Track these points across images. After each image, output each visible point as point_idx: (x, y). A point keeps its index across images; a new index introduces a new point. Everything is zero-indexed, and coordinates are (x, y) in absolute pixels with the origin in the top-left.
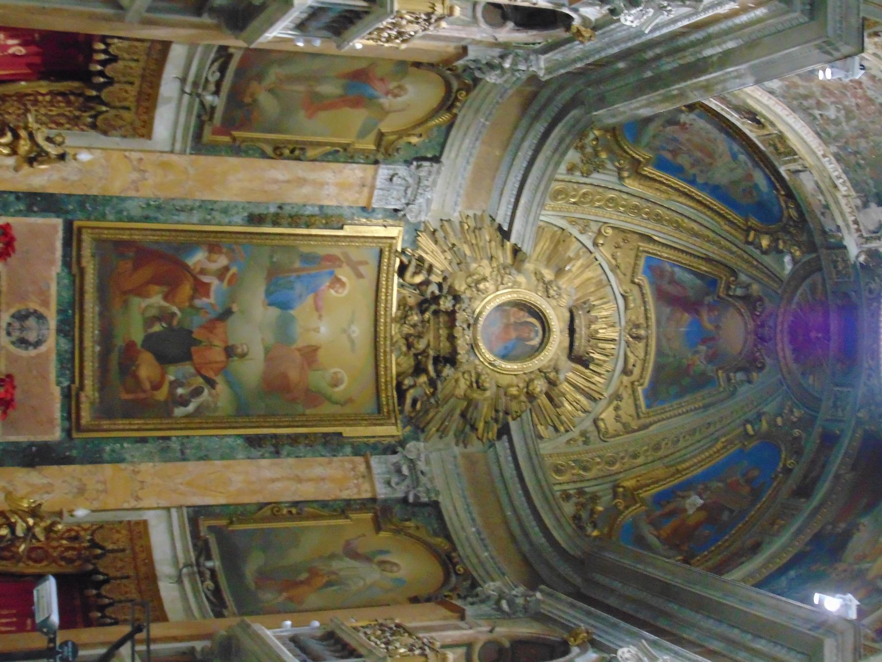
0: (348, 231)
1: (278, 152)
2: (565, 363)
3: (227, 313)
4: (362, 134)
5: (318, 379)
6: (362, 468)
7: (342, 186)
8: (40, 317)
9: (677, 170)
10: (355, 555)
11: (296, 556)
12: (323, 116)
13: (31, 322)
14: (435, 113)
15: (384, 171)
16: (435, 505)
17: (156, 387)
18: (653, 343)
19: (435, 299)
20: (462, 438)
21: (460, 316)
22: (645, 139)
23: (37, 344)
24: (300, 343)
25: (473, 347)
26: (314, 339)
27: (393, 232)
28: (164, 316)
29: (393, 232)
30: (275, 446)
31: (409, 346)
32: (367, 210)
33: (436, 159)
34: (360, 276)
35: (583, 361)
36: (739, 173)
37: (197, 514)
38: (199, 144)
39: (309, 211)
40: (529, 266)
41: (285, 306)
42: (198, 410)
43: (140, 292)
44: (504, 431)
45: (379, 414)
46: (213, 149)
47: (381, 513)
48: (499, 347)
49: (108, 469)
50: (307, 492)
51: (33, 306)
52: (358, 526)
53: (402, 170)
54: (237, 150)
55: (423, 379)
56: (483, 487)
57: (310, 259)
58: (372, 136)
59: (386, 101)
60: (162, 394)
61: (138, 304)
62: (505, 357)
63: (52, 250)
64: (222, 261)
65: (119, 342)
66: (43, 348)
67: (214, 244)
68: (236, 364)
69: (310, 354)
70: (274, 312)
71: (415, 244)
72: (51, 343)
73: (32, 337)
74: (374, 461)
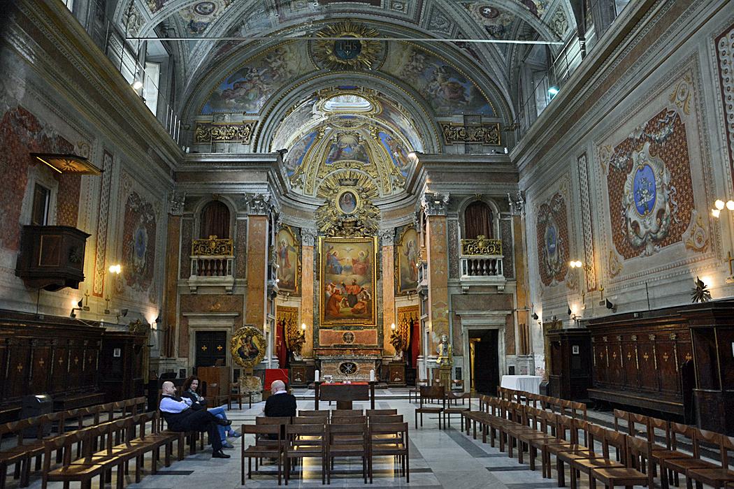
0: (320, 252)
1: (300, 273)
2: (357, 187)
4: (294, 251)
5: (362, 259)
6: (386, 248)
8: (345, 334)
9: (301, 158)
10: (408, 253)
11: (408, 268)
13: (346, 337)
14: (288, 231)
15: (304, 243)
16: (396, 228)
17: (364, 304)
19: (339, 227)
20: (378, 218)
21: (344, 220)
22: (292, 168)
25: (351, 215)
26: (350, 260)
27: (320, 239)
28: (344, 302)
29: (320, 239)
30: (379, 272)
31: (352, 233)
32: (315, 246)
33: (300, 229)
34: (332, 248)
35: (356, 181)
36: (303, 143)
37: (396, 294)
38: (300, 295)
39: (315, 264)
41: (341, 269)
43: (338, 308)
44: (376, 206)
45: (371, 242)
46: (300, 291)
50: (391, 264)
52: (402, 251)
53: (303, 238)
55: (361, 230)
56: (391, 214)
58: (295, 248)
59: (286, 246)
60: (365, 302)
62: (356, 204)
63: (327, 332)
64: (329, 286)
66: (353, 334)
68: (357, 282)
69: (354, 262)
71: (324, 232)
72: (351, 332)
73: (351, 336)
74: (384, 245)
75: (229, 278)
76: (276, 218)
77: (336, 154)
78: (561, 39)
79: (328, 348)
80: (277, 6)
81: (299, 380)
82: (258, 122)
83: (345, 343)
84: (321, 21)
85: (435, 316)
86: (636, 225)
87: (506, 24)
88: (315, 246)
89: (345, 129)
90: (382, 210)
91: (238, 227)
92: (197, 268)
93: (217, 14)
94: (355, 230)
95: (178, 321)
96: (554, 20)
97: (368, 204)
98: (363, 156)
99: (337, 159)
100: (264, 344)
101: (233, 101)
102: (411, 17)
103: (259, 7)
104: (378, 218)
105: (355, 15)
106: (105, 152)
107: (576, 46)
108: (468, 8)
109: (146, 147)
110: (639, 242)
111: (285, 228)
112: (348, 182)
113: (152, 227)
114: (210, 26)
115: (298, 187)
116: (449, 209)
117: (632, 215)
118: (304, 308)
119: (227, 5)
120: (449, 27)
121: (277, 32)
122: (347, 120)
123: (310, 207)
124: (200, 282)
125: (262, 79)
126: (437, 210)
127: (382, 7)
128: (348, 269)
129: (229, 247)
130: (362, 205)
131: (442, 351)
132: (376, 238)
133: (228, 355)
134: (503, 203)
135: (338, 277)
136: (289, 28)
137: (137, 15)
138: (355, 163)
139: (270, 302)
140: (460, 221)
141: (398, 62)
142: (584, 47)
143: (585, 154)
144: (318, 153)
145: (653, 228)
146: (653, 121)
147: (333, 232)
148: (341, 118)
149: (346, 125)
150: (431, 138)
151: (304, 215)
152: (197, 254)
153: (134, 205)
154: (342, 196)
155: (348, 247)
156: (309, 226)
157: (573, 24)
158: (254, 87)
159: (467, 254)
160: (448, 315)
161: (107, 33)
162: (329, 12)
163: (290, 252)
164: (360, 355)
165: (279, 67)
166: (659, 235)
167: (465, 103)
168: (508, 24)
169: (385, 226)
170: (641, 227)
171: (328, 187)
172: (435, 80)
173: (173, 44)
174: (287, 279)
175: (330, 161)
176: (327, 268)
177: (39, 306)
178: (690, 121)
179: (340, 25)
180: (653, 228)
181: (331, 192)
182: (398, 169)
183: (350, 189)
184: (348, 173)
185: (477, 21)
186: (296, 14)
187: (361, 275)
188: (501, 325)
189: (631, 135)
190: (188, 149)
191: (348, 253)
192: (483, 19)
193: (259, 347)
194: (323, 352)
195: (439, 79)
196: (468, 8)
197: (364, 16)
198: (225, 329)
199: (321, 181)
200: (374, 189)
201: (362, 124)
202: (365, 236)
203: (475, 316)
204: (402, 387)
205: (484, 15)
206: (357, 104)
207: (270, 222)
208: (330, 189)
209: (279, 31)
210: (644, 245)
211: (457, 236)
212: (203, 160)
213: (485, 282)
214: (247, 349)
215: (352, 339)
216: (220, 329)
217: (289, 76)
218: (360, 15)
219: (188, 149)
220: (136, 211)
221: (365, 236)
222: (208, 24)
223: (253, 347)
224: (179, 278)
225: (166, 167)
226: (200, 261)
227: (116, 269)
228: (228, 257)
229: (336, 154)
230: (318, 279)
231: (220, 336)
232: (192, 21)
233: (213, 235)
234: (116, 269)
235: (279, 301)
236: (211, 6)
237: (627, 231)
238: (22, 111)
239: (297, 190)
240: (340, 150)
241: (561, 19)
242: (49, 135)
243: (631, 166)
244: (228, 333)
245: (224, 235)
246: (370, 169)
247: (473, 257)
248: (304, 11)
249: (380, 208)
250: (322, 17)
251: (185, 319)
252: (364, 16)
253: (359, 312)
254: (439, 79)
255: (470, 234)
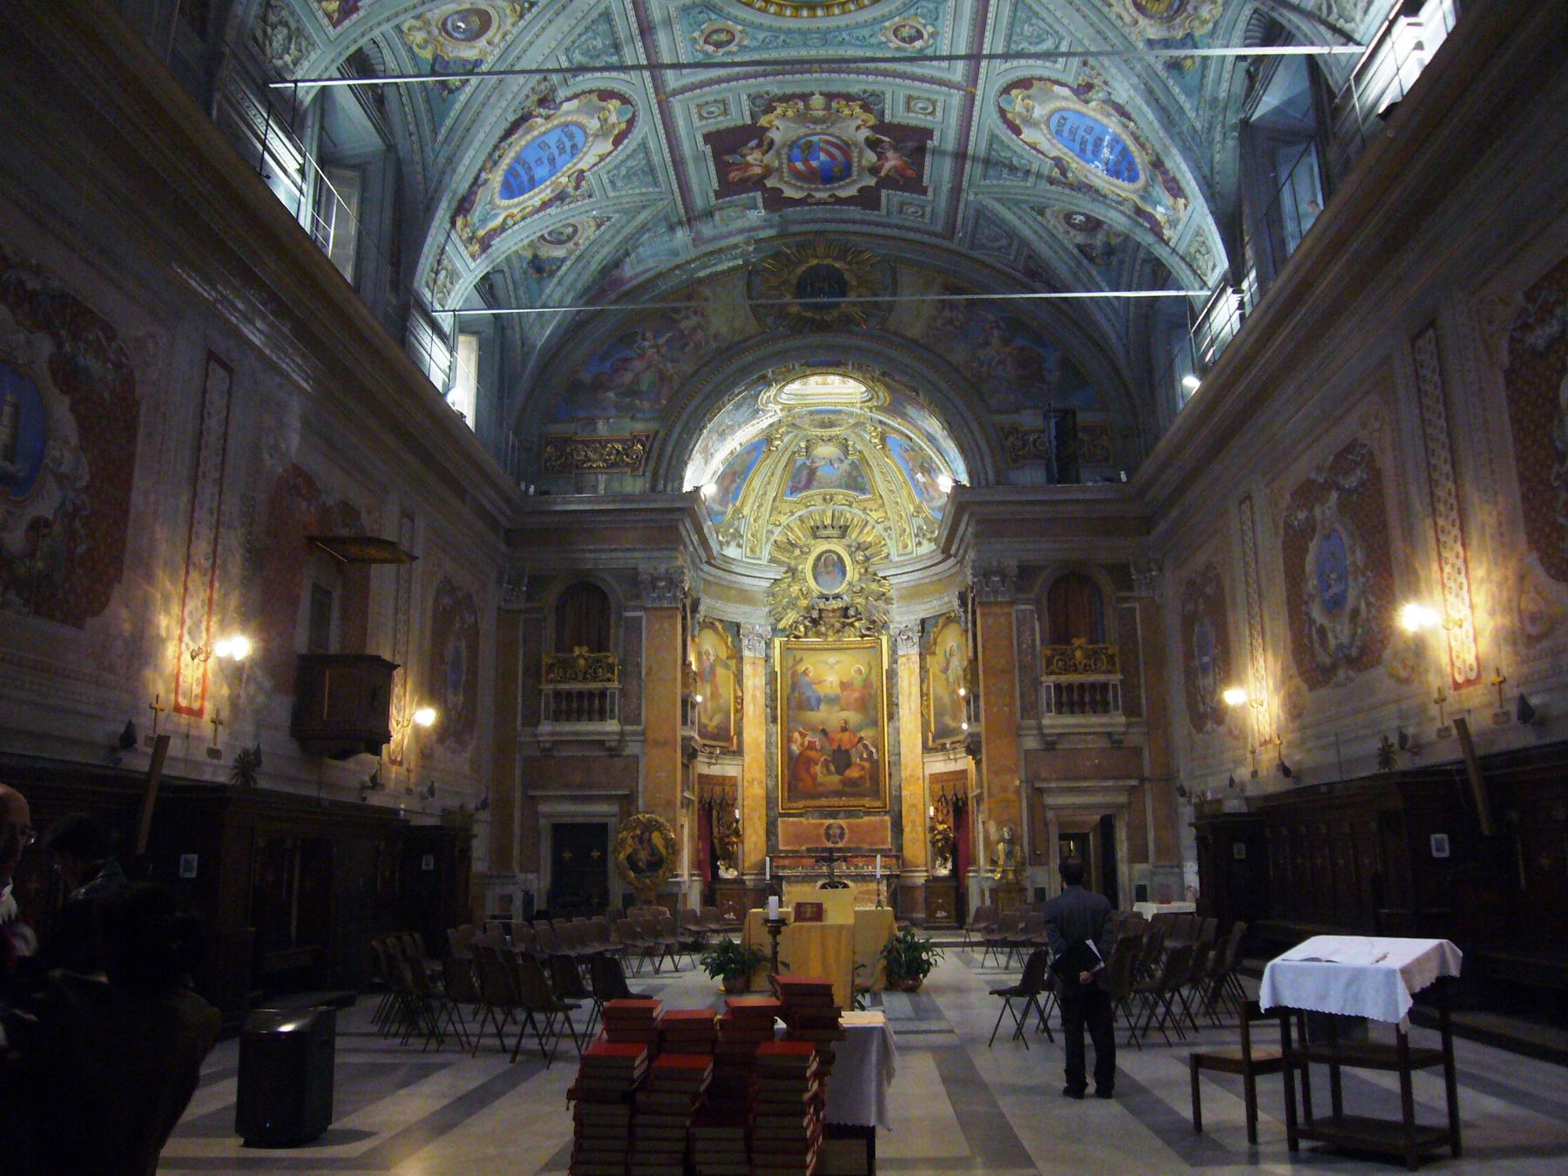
0: (778, 669)
1: (739, 711)
2: (846, 541)
3: (824, 732)
4: (727, 667)
5: (858, 682)
7: (755, 675)
8: (829, 827)
11: (946, 699)
12: (721, 691)
15: (746, 653)
16: (923, 622)
17: (863, 768)
18: (833, 491)
20: (889, 601)
21: (822, 606)
23: (841, 828)
24: (838, 691)
25: (837, 597)
26: (836, 683)
27: (777, 642)
28: (826, 764)
30: (893, 705)
32: (767, 659)
33: (738, 626)
35: (844, 530)
37: (926, 749)
38: (739, 752)
40: (793, 563)
41: (819, 700)
42: (876, 747)
43: (814, 777)
45: (877, 648)
46: (740, 743)
47: (926, 651)
48: (839, 577)
49: (904, 793)
50: (916, 691)
51: (822, 831)
54: (740, 733)
56: (914, 593)
57: (794, 687)
59: (712, 658)
60: (867, 765)
61: (820, 778)
62: (844, 574)
64: (796, 735)
65: (840, 787)
67: (788, 740)
68: (851, 726)
69: (844, 686)
70: (823, 707)
71: (784, 630)
72: (841, 822)
74: (900, 653)
75: (612, 726)
76: (695, 609)
77: (803, 478)
78: (1205, 283)
79: (795, 855)
80: (689, 220)
81: (732, 916)
82: (657, 433)
83: (830, 845)
84: (771, 238)
85: (995, 790)
86: (1322, 632)
87: (1114, 241)
88: (767, 659)
89: (819, 432)
90: (897, 582)
91: (627, 628)
92: (553, 707)
93: (496, 40)
94: (844, 625)
95: (518, 804)
96: (1192, 250)
97: (869, 574)
98: (856, 481)
99: (808, 486)
100: (673, 846)
101: (611, 394)
102: (939, 228)
103: (655, 225)
104: (889, 601)
105: (833, 226)
106: (212, 356)
107: (1230, 301)
108: (1042, 214)
109: (462, 493)
110: (1328, 661)
111: (709, 625)
112: (829, 532)
113: (473, 635)
114: (569, 263)
115: (733, 544)
116: (1019, 589)
117: (1316, 613)
118: (748, 777)
119: (599, 226)
120: (1010, 246)
121: (688, 262)
122: (827, 418)
123: (756, 582)
124: (560, 734)
125: (663, 351)
126: (995, 592)
127: (884, 211)
128: (832, 701)
129: (611, 668)
130: (857, 576)
131: (1002, 857)
132: (884, 639)
133: (611, 866)
134: (1122, 575)
135: (815, 717)
136: (712, 253)
137: (293, 25)
138: (841, 495)
139: (685, 766)
140: (1039, 611)
141: (915, 304)
142: (1241, 305)
143: (1249, 497)
144: (765, 481)
145: (1345, 639)
146: (1341, 455)
147: (802, 628)
148: (811, 413)
149: (823, 425)
150: (982, 455)
151: (745, 597)
152: (551, 681)
153: (446, 600)
154: (818, 558)
155: (832, 658)
156: (755, 620)
157: (1223, 264)
158: (648, 367)
159: (1052, 673)
160: (1018, 791)
161: (406, 310)
162: (786, 222)
163: (720, 671)
164: (856, 867)
165: (694, 329)
166: (1354, 652)
167: (1045, 387)
168: (1119, 240)
169: (903, 617)
170: (1330, 636)
171: (790, 543)
172: (987, 343)
173: (391, 95)
174: (715, 723)
175: (794, 490)
176: (791, 701)
177: (320, 784)
178: (1387, 463)
179: (806, 244)
180: (1345, 639)
181: (797, 552)
182: (925, 506)
183: (838, 547)
184: (829, 514)
185: (1060, 237)
186: (725, 230)
187: (857, 710)
188: (1120, 807)
189: (1313, 475)
190: (532, 489)
191: (832, 669)
192: (1073, 232)
193: (664, 851)
194: (786, 862)
195: (995, 340)
196: (1042, 214)
197: (850, 227)
198: (604, 820)
199: (777, 531)
200: (879, 543)
201: (852, 421)
202: (863, 636)
203: (1071, 790)
204: (948, 928)
205: (1074, 226)
206: (838, 390)
207: (684, 618)
208: (794, 546)
209: (693, 261)
210: (1334, 667)
211: (1034, 640)
212: (559, 508)
213: (1085, 726)
214: (643, 856)
215: (842, 836)
216: (596, 820)
217: (714, 345)
218: (843, 227)
219: (532, 489)
220: (451, 611)
221: (863, 636)
222: (563, 260)
223: (654, 851)
224: (519, 727)
225: (492, 523)
226: (558, 694)
227: (238, 646)
228: (608, 685)
229: (803, 478)
230: (774, 720)
231: (596, 833)
232: (535, 257)
233: (580, 645)
234: (238, 646)
235: (702, 767)
236: (570, 230)
237: (1311, 641)
238: (297, 470)
239: (732, 552)
240: (812, 472)
241: (1203, 250)
242: (330, 502)
243: (1314, 529)
244: (611, 828)
245: (600, 645)
246: (870, 505)
247: (1064, 679)
248: (739, 224)
249: (894, 581)
250: (772, 232)
251: (531, 801)
252: (850, 227)
253: (853, 783)
254: (995, 340)
255: (1060, 635)
